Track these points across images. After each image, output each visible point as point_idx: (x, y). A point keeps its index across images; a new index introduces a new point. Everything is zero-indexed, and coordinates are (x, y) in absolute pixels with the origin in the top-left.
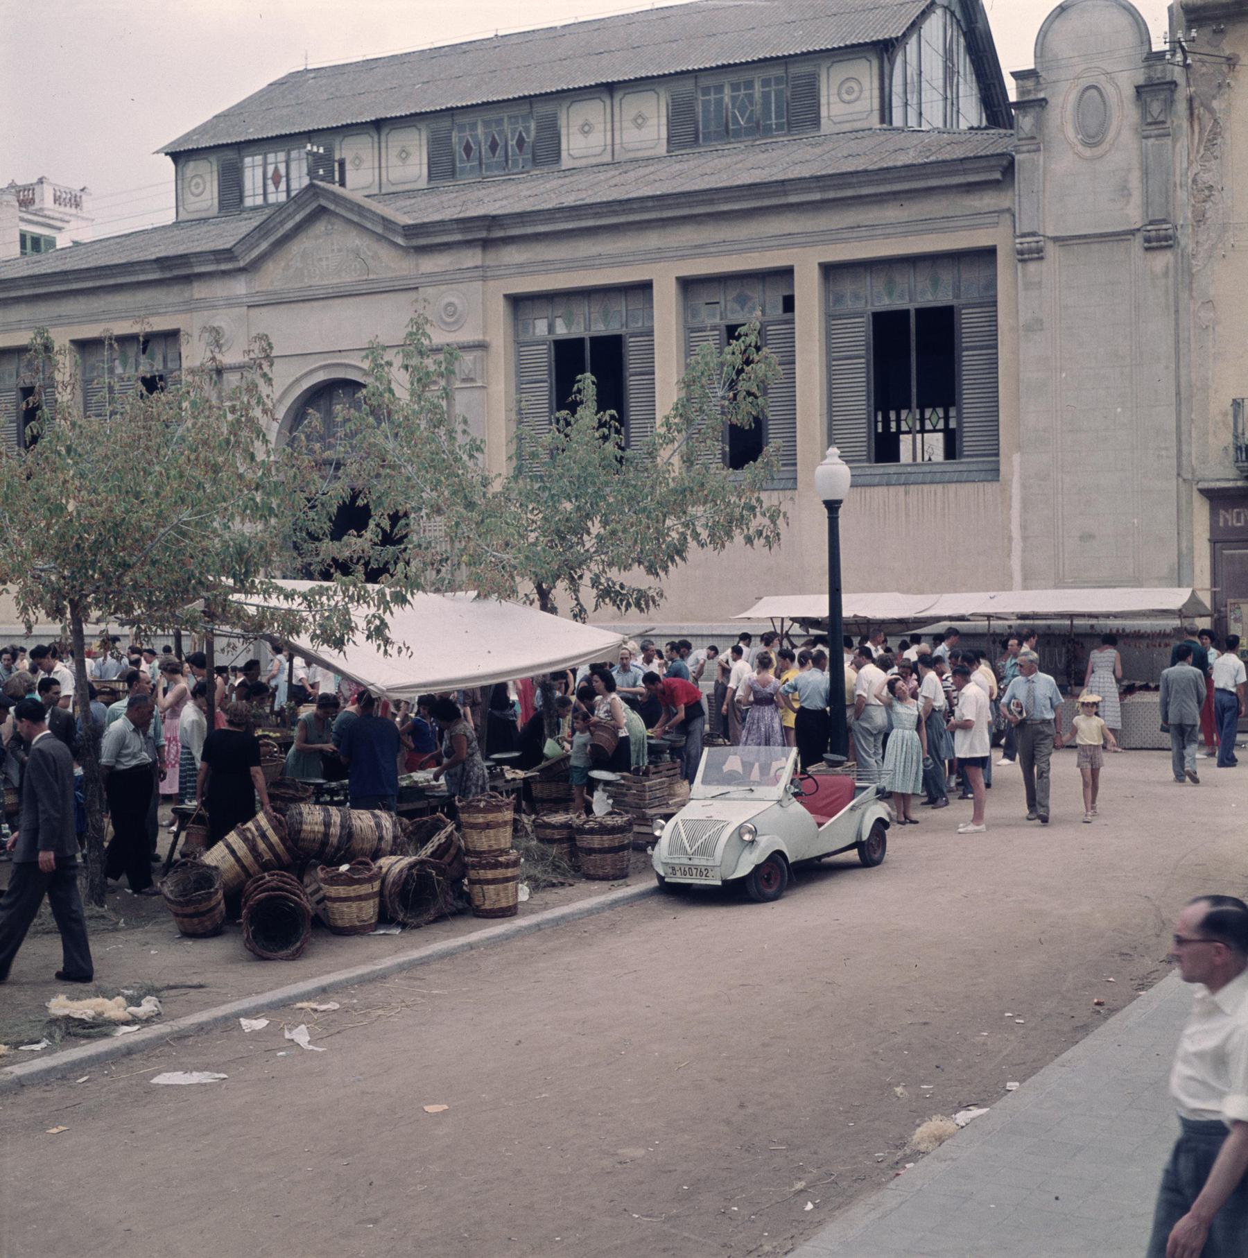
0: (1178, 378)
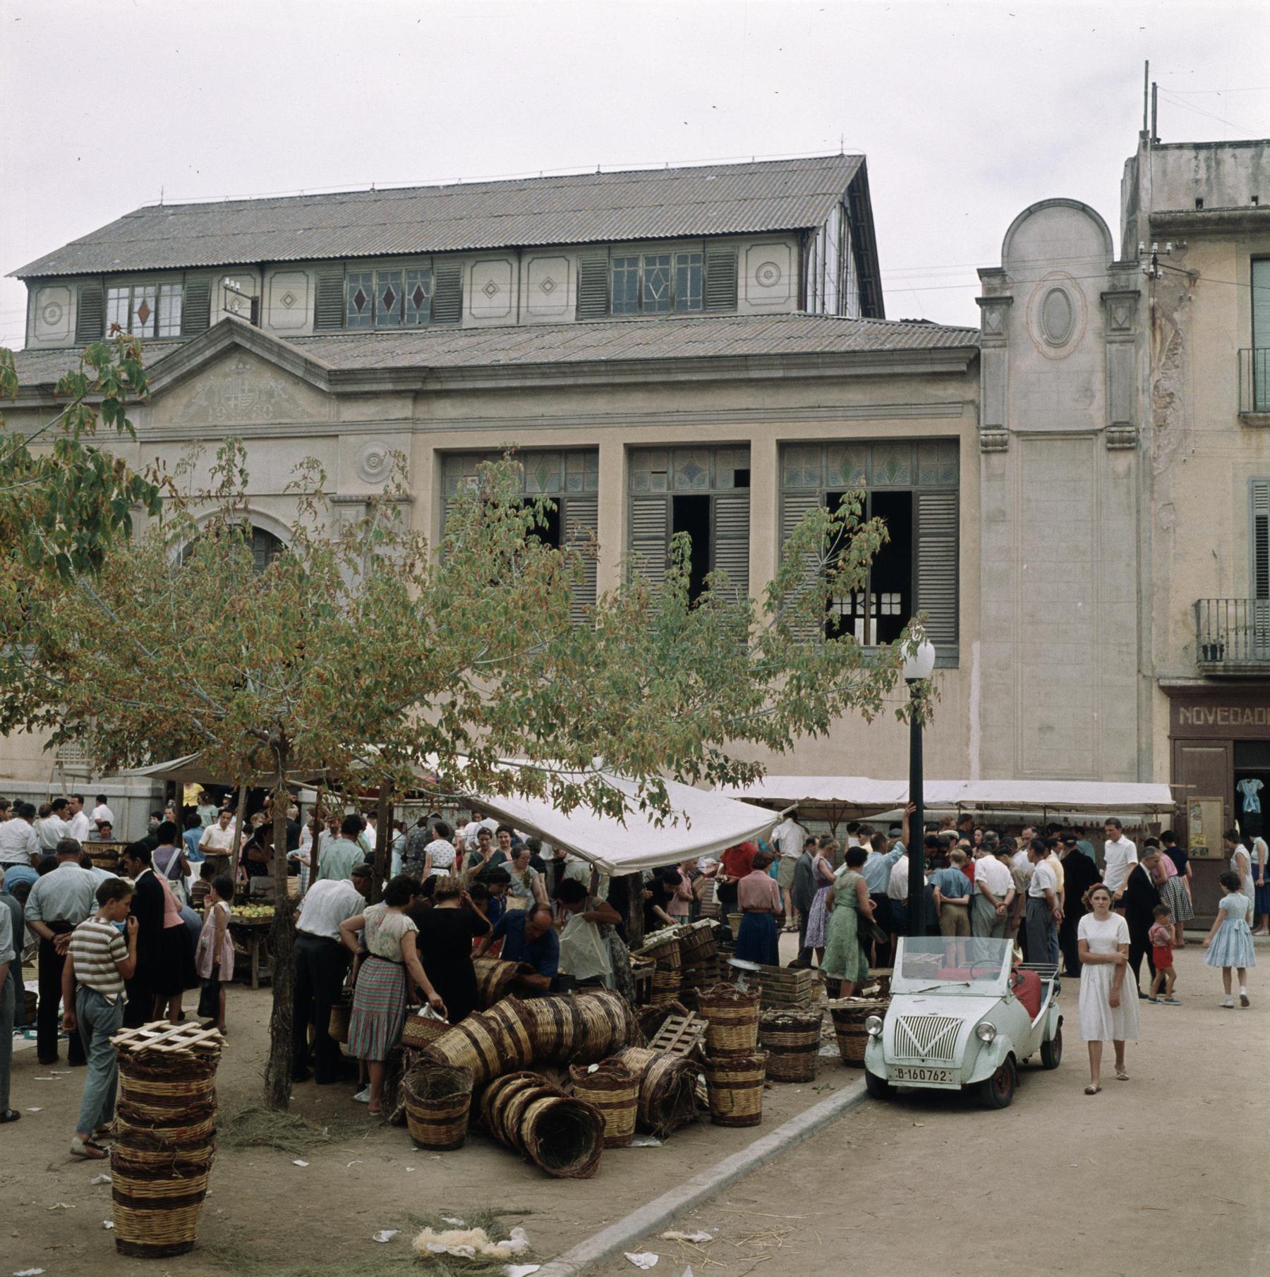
0: (1139, 574)
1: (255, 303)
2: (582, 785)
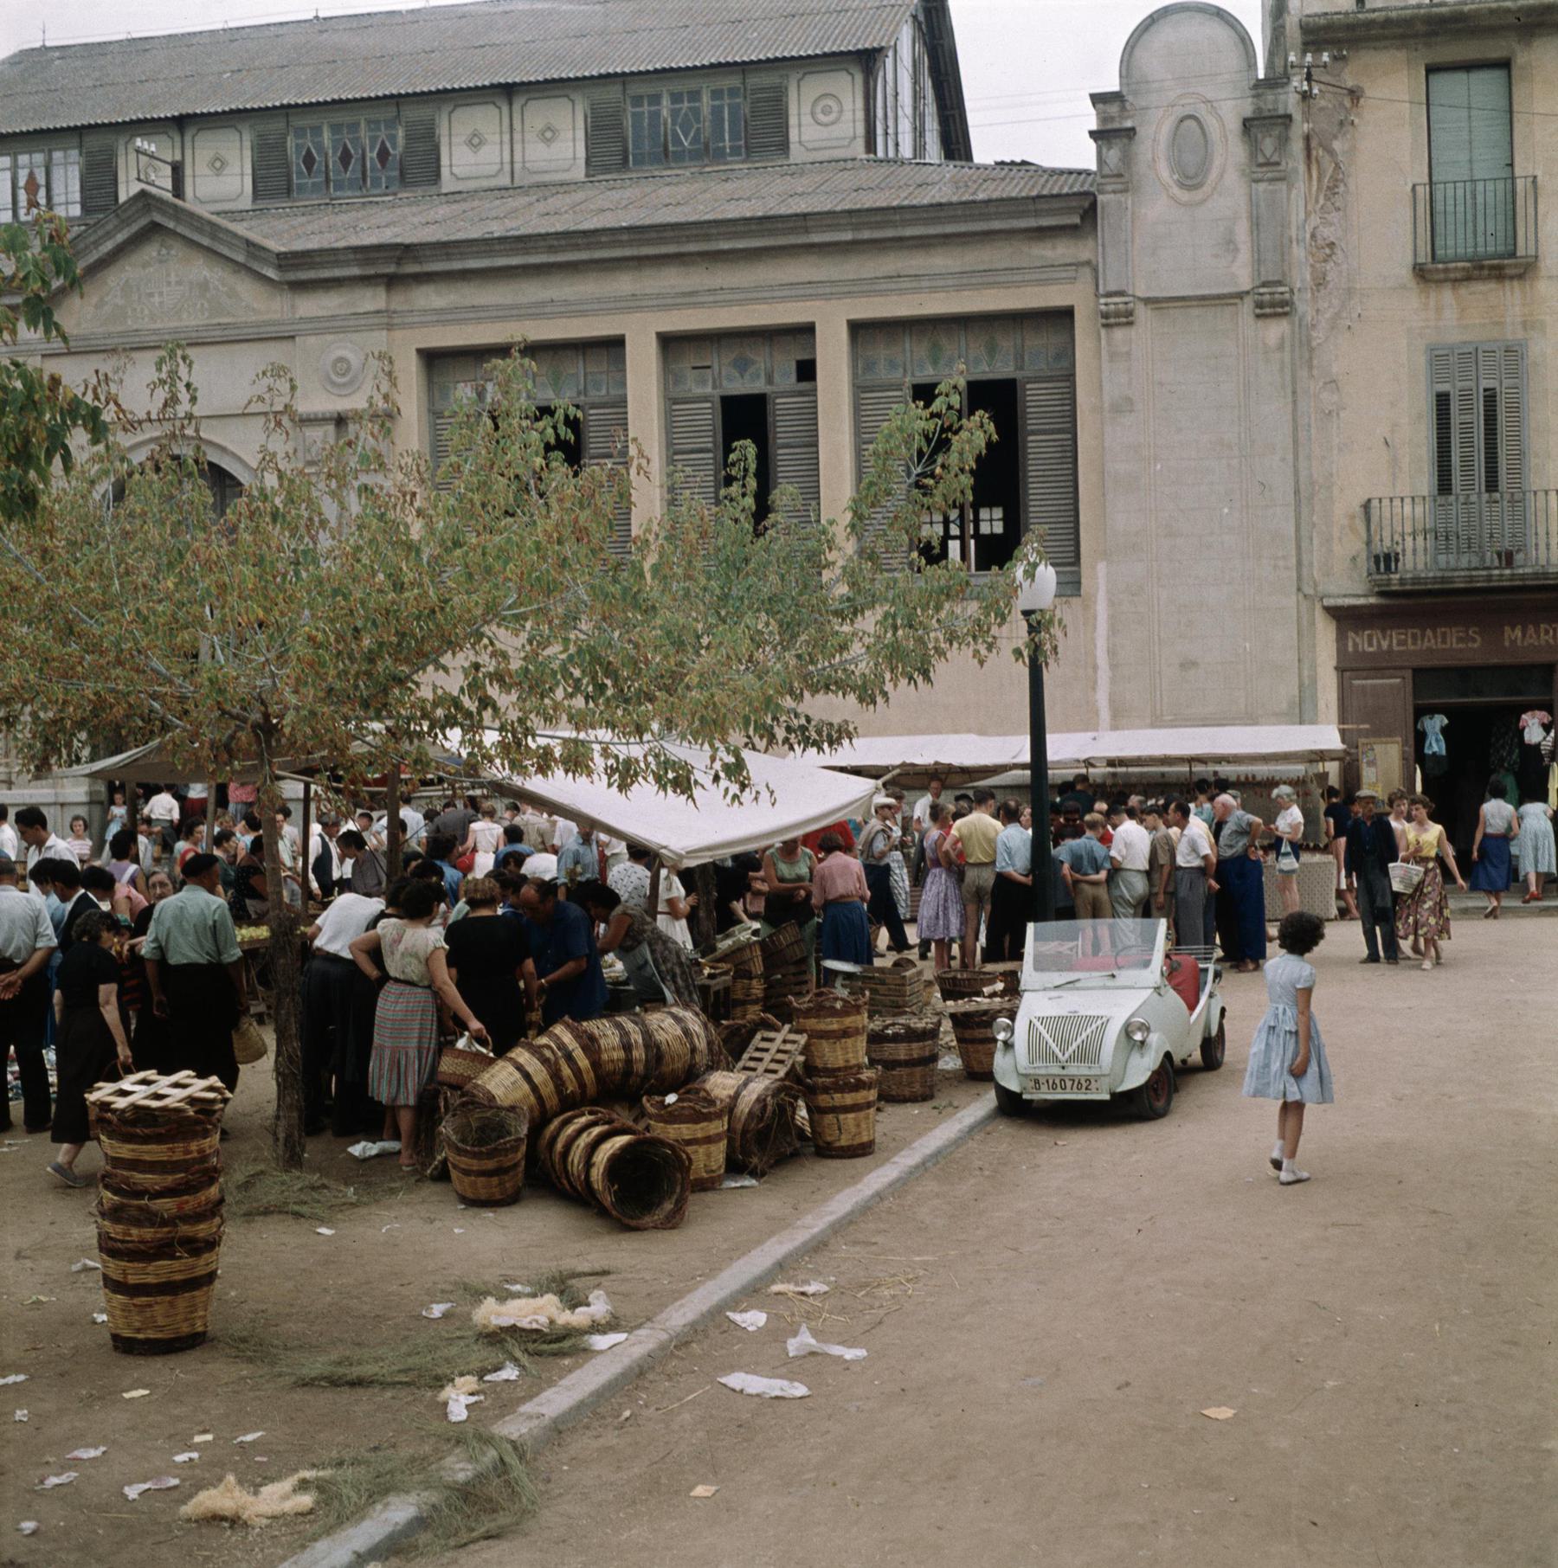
1: (177, 170)
2: (641, 758)
